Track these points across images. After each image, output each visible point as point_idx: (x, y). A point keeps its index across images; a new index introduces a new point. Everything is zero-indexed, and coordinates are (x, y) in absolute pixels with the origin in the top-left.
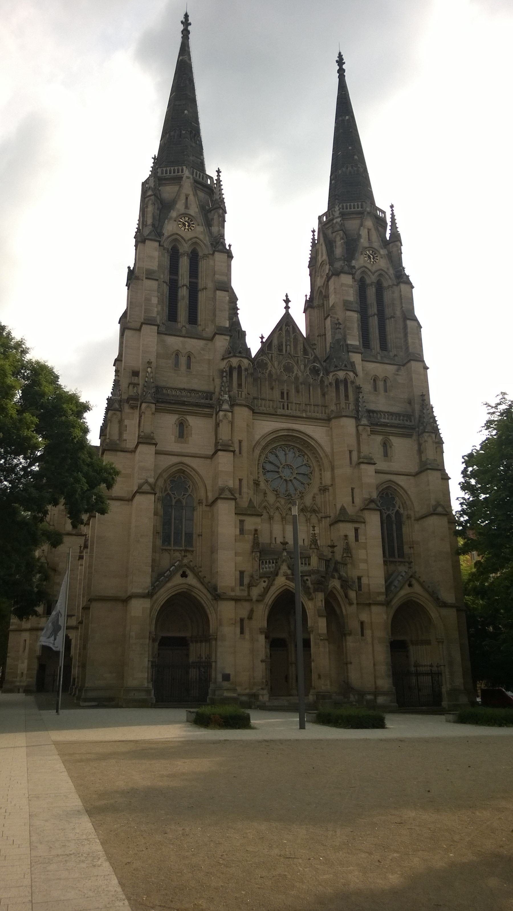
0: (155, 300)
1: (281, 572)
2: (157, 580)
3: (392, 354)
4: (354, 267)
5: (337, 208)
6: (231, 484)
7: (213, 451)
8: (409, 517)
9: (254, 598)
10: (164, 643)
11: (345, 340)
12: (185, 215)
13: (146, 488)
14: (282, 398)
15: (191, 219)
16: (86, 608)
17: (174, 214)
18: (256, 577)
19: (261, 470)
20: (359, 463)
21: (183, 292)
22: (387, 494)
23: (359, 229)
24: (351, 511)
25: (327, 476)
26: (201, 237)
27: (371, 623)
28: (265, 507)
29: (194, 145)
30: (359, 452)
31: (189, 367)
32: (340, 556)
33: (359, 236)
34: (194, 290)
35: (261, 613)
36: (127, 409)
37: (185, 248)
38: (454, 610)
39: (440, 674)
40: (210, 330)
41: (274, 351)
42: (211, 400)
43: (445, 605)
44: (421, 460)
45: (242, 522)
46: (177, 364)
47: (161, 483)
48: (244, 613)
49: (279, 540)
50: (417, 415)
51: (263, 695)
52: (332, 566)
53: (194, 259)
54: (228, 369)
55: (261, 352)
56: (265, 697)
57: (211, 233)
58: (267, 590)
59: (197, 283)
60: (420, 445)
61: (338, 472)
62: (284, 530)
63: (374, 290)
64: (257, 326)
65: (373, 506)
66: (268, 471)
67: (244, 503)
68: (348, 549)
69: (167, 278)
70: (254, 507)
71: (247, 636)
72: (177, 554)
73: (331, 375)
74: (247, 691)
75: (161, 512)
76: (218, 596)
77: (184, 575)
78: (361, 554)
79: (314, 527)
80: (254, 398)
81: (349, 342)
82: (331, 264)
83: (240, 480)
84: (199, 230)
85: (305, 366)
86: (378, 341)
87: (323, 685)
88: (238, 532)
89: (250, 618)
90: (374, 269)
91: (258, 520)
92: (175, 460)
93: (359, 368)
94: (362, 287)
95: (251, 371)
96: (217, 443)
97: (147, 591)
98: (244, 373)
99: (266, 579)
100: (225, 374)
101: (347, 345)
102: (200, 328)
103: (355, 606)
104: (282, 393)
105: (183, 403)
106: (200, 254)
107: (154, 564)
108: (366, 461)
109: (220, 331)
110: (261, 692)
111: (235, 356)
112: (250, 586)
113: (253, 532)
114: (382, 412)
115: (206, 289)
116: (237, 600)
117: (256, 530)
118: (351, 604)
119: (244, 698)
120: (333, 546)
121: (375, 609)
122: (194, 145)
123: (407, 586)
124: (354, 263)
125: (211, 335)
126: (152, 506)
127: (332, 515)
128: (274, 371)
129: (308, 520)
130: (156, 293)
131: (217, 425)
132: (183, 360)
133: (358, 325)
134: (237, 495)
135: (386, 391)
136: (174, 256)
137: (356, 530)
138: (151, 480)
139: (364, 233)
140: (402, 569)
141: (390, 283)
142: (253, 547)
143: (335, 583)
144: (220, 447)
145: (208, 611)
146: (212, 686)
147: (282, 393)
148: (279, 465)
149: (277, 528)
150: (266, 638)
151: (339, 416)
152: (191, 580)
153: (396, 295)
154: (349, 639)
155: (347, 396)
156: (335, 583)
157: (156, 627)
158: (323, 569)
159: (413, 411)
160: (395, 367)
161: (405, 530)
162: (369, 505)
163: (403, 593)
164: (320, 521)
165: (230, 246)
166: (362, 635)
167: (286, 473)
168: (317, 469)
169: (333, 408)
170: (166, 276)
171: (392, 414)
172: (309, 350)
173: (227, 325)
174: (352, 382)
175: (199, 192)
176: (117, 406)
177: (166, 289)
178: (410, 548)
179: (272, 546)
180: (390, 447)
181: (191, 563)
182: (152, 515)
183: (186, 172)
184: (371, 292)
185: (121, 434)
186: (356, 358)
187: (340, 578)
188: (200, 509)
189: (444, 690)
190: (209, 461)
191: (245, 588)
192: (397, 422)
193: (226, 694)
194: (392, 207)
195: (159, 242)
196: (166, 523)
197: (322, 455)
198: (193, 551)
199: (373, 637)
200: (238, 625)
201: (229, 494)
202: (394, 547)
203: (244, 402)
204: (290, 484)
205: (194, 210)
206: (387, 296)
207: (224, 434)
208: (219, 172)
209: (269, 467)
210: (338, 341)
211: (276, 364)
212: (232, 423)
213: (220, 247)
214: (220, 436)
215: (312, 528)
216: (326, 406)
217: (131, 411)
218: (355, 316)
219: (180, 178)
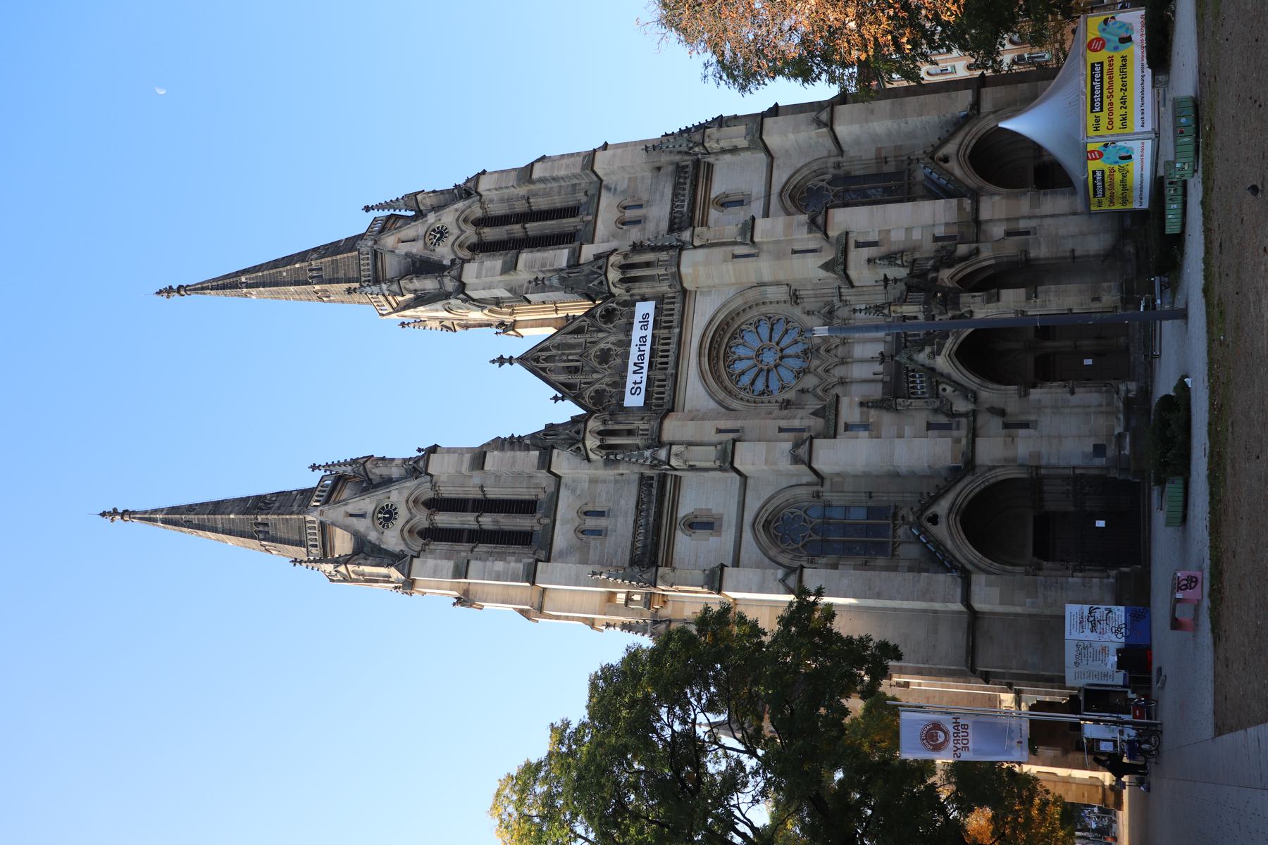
0: (499, 566)
1: (927, 362)
2: (941, 564)
3: (584, 199)
4: (453, 261)
6: (788, 446)
7: (734, 475)
8: (838, 166)
9: (970, 407)
10: (1043, 551)
11: (561, 270)
13: (792, 581)
17: (373, 536)
18: (937, 404)
19: (765, 398)
21: (488, 521)
23: (398, 255)
24: (827, 256)
25: (774, 293)
26: (406, 493)
27: (1008, 220)
28: (825, 391)
29: (277, 504)
30: (735, 243)
31: (601, 514)
32: (902, 269)
33: (407, 255)
34: (484, 505)
35: (991, 394)
37: (422, 519)
38: (983, 90)
40: (543, 477)
41: (575, 379)
42: (652, 478)
43: (976, 105)
44: (748, 149)
45: (848, 427)
46: (597, 532)
48: (995, 423)
49: (879, 368)
50: (677, 158)
51: (1128, 391)
53: (438, 504)
54: (604, 452)
55: (577, 400)
58: (957, 386)
59: (475, 500)
60: (723, 151)
61: (767, 278)
62: (863, 361)
63: (487, 230)
64: (538, 407)
65: (820, 220)
66: (767, 387)
67: (818, 423)
68: (890, 258)
69: (468, 546)
70: (824, 407)
72: (901, 532)
73: (614, 290)
74: (1121, 416)
75: (832, 558)
76: (967, 466)
77: (934, 520)
78: (898, 237)
79: (855, 311)
81: (564, 264)
83: (781, 430)
84: (397, 496)
85: (601, 331)
86: (564, 221)
87: (1110, 298)
89: (1002, 413)
91: (844, 402)
92: (748, 535)
94: (482, 248)
96: (721, 469)
97: (959, 580)
98: (611, 426)
99: (941, 387)
100: (612, 457)
101: (569, 266)
102: (542, 496)
103: (981, 245)
106: (431, 495)
107: (916, 568)
108: (748, 236)
109: (545, 463)
111: (584, 439)
112: (951, 414)
113: (865, 409)
114: (672, 209)
115: (482, 487)
116: (974, 434)
120: (886, 279)
121: (985, 214)
122: (277, 504)
123: (947, 165)
124: (447, 262)
126: (822, 572)
127: (836, 285)
128: (607, 380)
130: (489, 564)
131: (692, 468)
132: (591, 523)
134: (806, 435)
135: (640, 206)
136: (433, 534)
137: (859, 245)
138: (780, 573)
139: (404, 249)
140: (920, 174)
143: (945, 274)
144: (727, 461)
145: (992, 481)
146: (1114, 474)
148: (755, 370)
149: (859, 371)
150: (1034, 387)
151: (678, 276)
152: (942, 507)
153: (494, 195)
154: (1033, 254)
155: (648, 265)
157: (1019, 565)
159: (672, 163)
160: (603, 192)
161: (858, 171)
162: (818, 225)
163: (958, 172)
164: (846, 303)
165: (419, 450)
166: (1027, 233)
167: (770, 358)
168: (763, 309)
170: (464, 547)
171: (675, 195)
173: (537, 453)
174: (626, 256)
177: (482, 548)
178: (886, 162)
179: (888, 379)
180: (727, 196)
181: (915, 509)
184: (490, 234)
186: (588, 252)
187: (936, 269)
188: (827, 496)
190: (750, 482)
192: (687, 187)
194: (367, 209)
195: (413, 557)
198: (896, 507)
199: (1030, 218)
200: (1013, 431)
201: (802, 454)
202: (890, 181)
203: (655, 424)
204: (787, 352)
205: (367, 504)
206: (496, 209)
207: (705, 456)
208: (314, 467)
209: (760, 385)
210: (562, 280)
211: (595, 376)
212: (690, 444)
214: (710, 464)
215: (857, 314)
217: (670, 604)
218: (525, 257)
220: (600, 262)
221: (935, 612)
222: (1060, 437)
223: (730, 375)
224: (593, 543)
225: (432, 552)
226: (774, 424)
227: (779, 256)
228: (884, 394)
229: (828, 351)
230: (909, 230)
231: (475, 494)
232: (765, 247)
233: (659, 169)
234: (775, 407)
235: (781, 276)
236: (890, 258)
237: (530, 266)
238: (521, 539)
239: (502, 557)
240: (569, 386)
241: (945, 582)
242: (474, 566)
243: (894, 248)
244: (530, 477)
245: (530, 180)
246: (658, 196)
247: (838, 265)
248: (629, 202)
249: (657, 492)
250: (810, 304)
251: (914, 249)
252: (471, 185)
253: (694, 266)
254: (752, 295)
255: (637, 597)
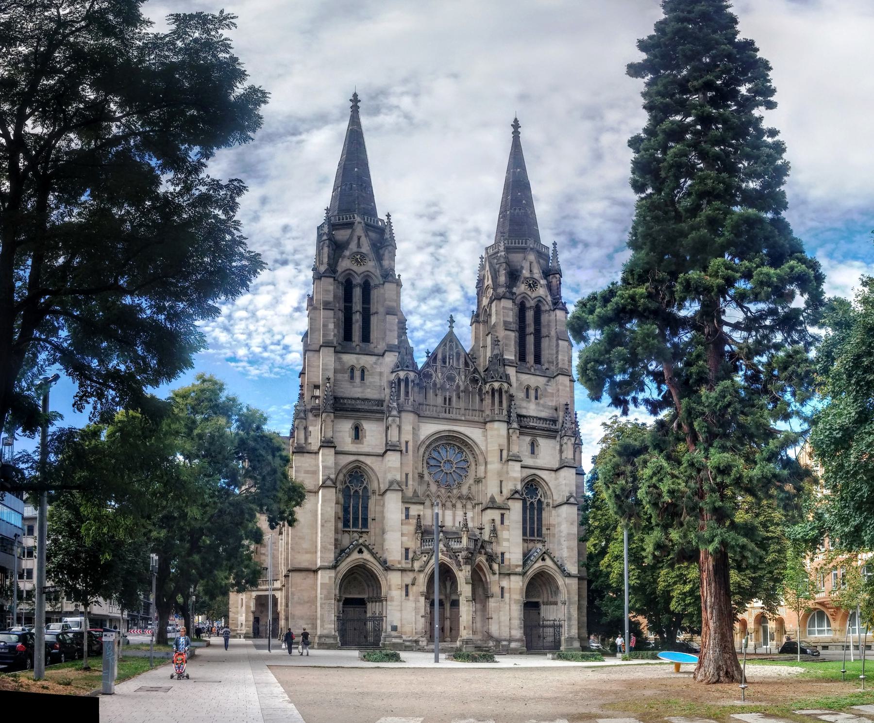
0: (331, 326)
3: (544, 367)
5: (502, 244)
6: (398, 478)
8: (548, 505)
10: (348, 602)
12: (358, 253)
13: (329, 483)
14: (445, 404)
15: (363, 256)
16: (286, 576)
17: (347, 253)
18: (418, 553)
19: (425, 465)
20: (508, 461)
22: (532, 485)
24: (499, 499)
25: (482, 468)
26: (372, 270)
28: (428, 496)
30: (509, 450)
31: (363, 379)
33: (522, 268)
35: (422, 579)
36: (310, 416)
37: (357, 280)
38: (577, 579)
39: (560, 626)
41: (439, 363)
43: (569, 575)
45: (407, 509)
46: (352, 378)
47: (341, 477)
50: (561, 421)
52: (479, 544)
53: (367, 288)
55: (427, 364)
56: (423, 643)
57: (381, 266)
59: (369, 308)
60: (561, 446)
65: (517, 496)
67: (410, 493)
68: (494, 531)
69: (342, 307)
71: (411, 597)
72: (355, 535)
73: (488, 385)
75: (342, 501)
76: (387, 568)
78: (504, 534)
80: (420, 404)
81: (505, 357)
82: (494, 289)
83: (407, 475)
88: (404, 518)
90: (533, 296)
91: (421, 507)
92: (352, 458)
93: (513, 379)
95: (417, 381)
96: (387, 443)
98: (411, 385)
102: (372, 346)
103: (497, 576)
104: (445, 399)
105: (358, 410)
106: (372, 284)
110: (421, 639)
111: (402, 370)
112: (413, 560)
116: (403, 570)
117: (419, 516)
118: (494, 574)
119: (408, 644)
120: (481, 529)
121: (513, 578)
124: (515, 290)
125: (381, 352)
126: (334, 498)
127: (484, 502)
128: (438, 381)
129: (464, 506)
130: (332, 320)
131: (387, 428)
132: (357, 374)
133: (515, 342)
134: (404, 487)
135: (536, 398)
137: (502, 515)
138: (333, 476)
139: (526, 265)
141: (547, 308)
142: (417, 530)
143: (482, 559)
144: (391, 448)
146: (383, 634)
147: (445, 399)
152: (366, 555)
153: (553, 317)
155: (501, 402)
156: (482, 559)
158: (472, 546)
160: (547, 379)
163: (536, 565)
164: (474, 507)
166: (502, 597)
167: (446, 468)
169: (488, 412)
172: (470, 363)
174: (506, 392)
175: (370, 234)
176: (302, 415)
177: (341, 315)
182: (333, 505)
183: (358, 219)
184: (530, 315)
185: (306, 439)
186: (511, 371)
189: (563, 638)
190: (380, 458)
191: (410, 561)
192: (544, 425)
193: (394, 640)
196: (346, 510)
197: (478, 452)
200: (404, 589)
201: (395, 486)
203: (410, 409)
205: (366, 248)
206: (544, 318)
208: (388, 216)
209: (432, 462)
212: (399, 427)
213: (390, 278)
214: (389, 439)
216: (482, 411)
218: (513, 335)
219: (353, 224)
220: (504, 378)
221: (316, 552)
222: (401, 610)
223: (438, 446)
224: (346, 375)
225: (338, 288)
226: (409, 469)
227: (500, 474)
228: (425, 526)
229: (449, 497)
230: (508, 540)
231: (373, 309)
232: (505, 467)
233: (556, 410)
234: (420, 470)
235: (489, 474)
236: (494, 531)
237: (507, 337)
238: (348, 336)
239: (336, 325)
240: (435, 358)
241: (331, 556)
242: (330, 313)
243: (499, 533)
244: (384, 339)
245: (558, 339)
246: (541, 408)
247: (492, 505)
248: (539, 393)
249: (376, 410)
250: (474, 488)
251: (498, 543)
252: (561, 306)
253: (499, 430)
254: (481, 459)
255: (317, 401)
